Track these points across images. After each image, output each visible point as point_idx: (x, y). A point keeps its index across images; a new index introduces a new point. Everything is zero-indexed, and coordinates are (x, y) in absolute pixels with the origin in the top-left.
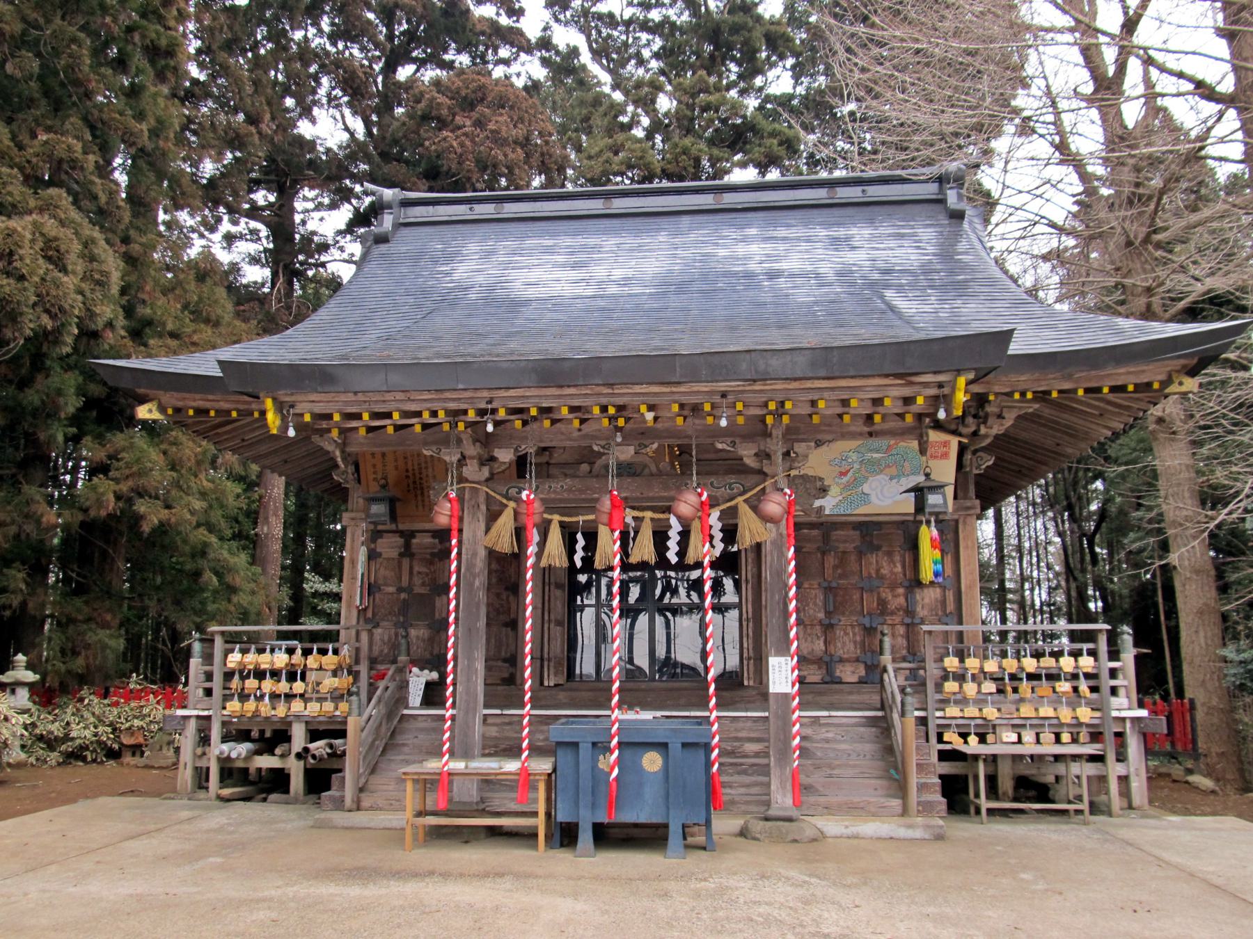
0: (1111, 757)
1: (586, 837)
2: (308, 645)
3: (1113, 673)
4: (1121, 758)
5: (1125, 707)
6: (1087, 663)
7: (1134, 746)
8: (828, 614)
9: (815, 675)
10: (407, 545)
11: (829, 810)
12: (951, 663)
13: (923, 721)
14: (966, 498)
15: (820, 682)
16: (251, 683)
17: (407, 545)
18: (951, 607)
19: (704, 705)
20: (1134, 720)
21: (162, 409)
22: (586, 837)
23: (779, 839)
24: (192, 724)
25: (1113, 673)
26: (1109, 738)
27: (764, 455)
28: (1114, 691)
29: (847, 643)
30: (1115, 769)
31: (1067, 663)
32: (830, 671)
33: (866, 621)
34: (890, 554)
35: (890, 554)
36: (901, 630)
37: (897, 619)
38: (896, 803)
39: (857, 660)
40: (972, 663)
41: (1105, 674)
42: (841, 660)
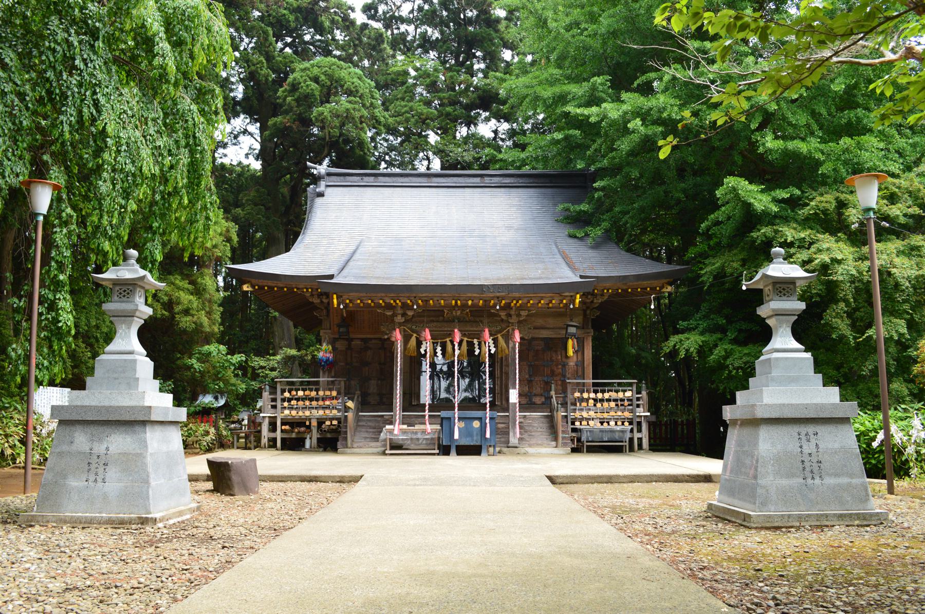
0: (635, 430)
1: (453, 451)
2: (283, 387)
3: (638, 399)
4: (640, 431)
5: (642, 412)
6: (628, 394)
7: (644, 427)
8: (530, 376)
9: (524, 401)
10: (349, 345)
11: (530, 446)
12: (577, 395)
13: (566, 417)
14: (588, 328)
15: (527, 404)
16: (307, 403)
17: (349, 345)
18: (580, 373)
19: (425, 424)
20: (645, 416)
21: (253, 286)
22: (453, 451)
23: (512, 454)
24: (267, 420)
25: (638, 399)
26: (635, 424)
27: (509, 315)
28: (638, 406)
29: (537, 389)
30: (637, 435)
31: (592, 395)
32: (530, 400)
33: (546, 379)
34: (556, 352)
35: (556, 352)
36: (560, 383)
37: (558, 378)
38: (554, 443)
39: (542, 395)
40: (321, 393)
41: (635, 400)
42: (535, 395)
